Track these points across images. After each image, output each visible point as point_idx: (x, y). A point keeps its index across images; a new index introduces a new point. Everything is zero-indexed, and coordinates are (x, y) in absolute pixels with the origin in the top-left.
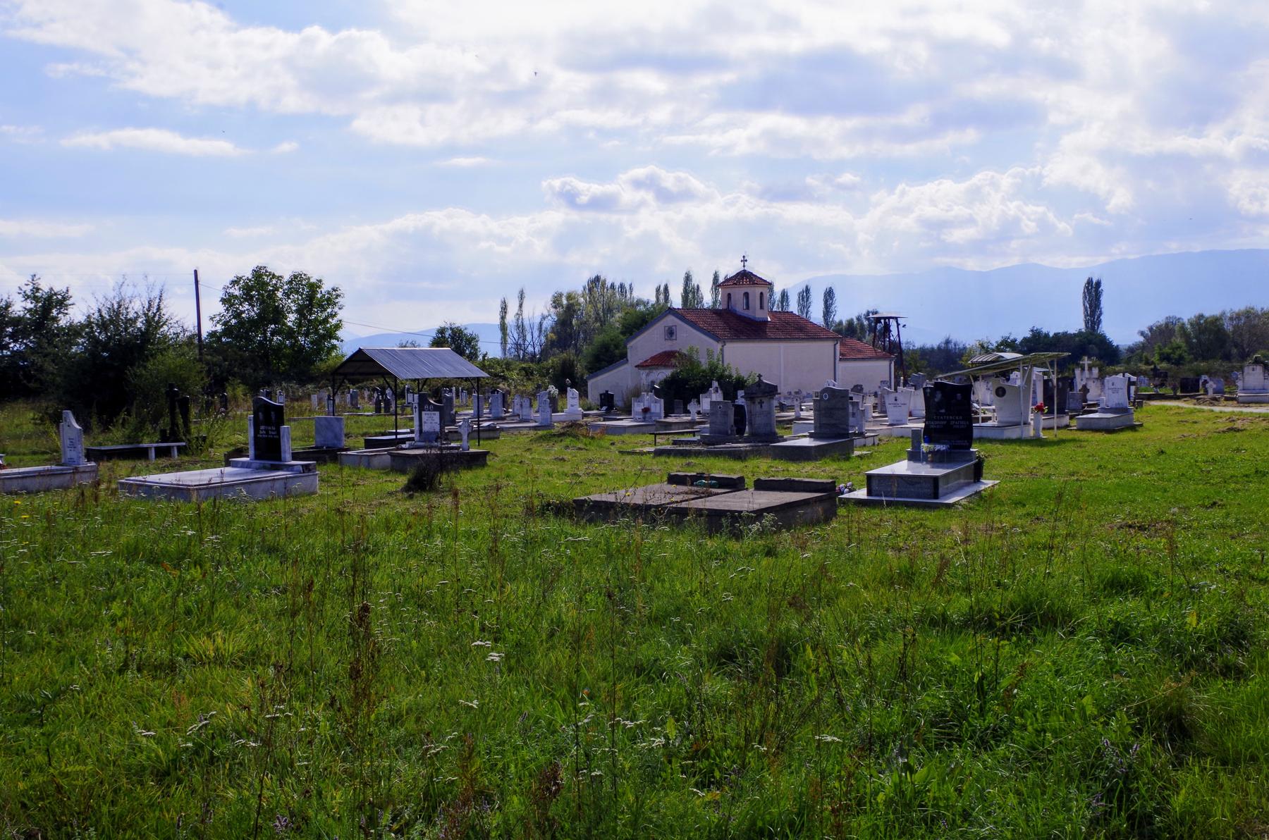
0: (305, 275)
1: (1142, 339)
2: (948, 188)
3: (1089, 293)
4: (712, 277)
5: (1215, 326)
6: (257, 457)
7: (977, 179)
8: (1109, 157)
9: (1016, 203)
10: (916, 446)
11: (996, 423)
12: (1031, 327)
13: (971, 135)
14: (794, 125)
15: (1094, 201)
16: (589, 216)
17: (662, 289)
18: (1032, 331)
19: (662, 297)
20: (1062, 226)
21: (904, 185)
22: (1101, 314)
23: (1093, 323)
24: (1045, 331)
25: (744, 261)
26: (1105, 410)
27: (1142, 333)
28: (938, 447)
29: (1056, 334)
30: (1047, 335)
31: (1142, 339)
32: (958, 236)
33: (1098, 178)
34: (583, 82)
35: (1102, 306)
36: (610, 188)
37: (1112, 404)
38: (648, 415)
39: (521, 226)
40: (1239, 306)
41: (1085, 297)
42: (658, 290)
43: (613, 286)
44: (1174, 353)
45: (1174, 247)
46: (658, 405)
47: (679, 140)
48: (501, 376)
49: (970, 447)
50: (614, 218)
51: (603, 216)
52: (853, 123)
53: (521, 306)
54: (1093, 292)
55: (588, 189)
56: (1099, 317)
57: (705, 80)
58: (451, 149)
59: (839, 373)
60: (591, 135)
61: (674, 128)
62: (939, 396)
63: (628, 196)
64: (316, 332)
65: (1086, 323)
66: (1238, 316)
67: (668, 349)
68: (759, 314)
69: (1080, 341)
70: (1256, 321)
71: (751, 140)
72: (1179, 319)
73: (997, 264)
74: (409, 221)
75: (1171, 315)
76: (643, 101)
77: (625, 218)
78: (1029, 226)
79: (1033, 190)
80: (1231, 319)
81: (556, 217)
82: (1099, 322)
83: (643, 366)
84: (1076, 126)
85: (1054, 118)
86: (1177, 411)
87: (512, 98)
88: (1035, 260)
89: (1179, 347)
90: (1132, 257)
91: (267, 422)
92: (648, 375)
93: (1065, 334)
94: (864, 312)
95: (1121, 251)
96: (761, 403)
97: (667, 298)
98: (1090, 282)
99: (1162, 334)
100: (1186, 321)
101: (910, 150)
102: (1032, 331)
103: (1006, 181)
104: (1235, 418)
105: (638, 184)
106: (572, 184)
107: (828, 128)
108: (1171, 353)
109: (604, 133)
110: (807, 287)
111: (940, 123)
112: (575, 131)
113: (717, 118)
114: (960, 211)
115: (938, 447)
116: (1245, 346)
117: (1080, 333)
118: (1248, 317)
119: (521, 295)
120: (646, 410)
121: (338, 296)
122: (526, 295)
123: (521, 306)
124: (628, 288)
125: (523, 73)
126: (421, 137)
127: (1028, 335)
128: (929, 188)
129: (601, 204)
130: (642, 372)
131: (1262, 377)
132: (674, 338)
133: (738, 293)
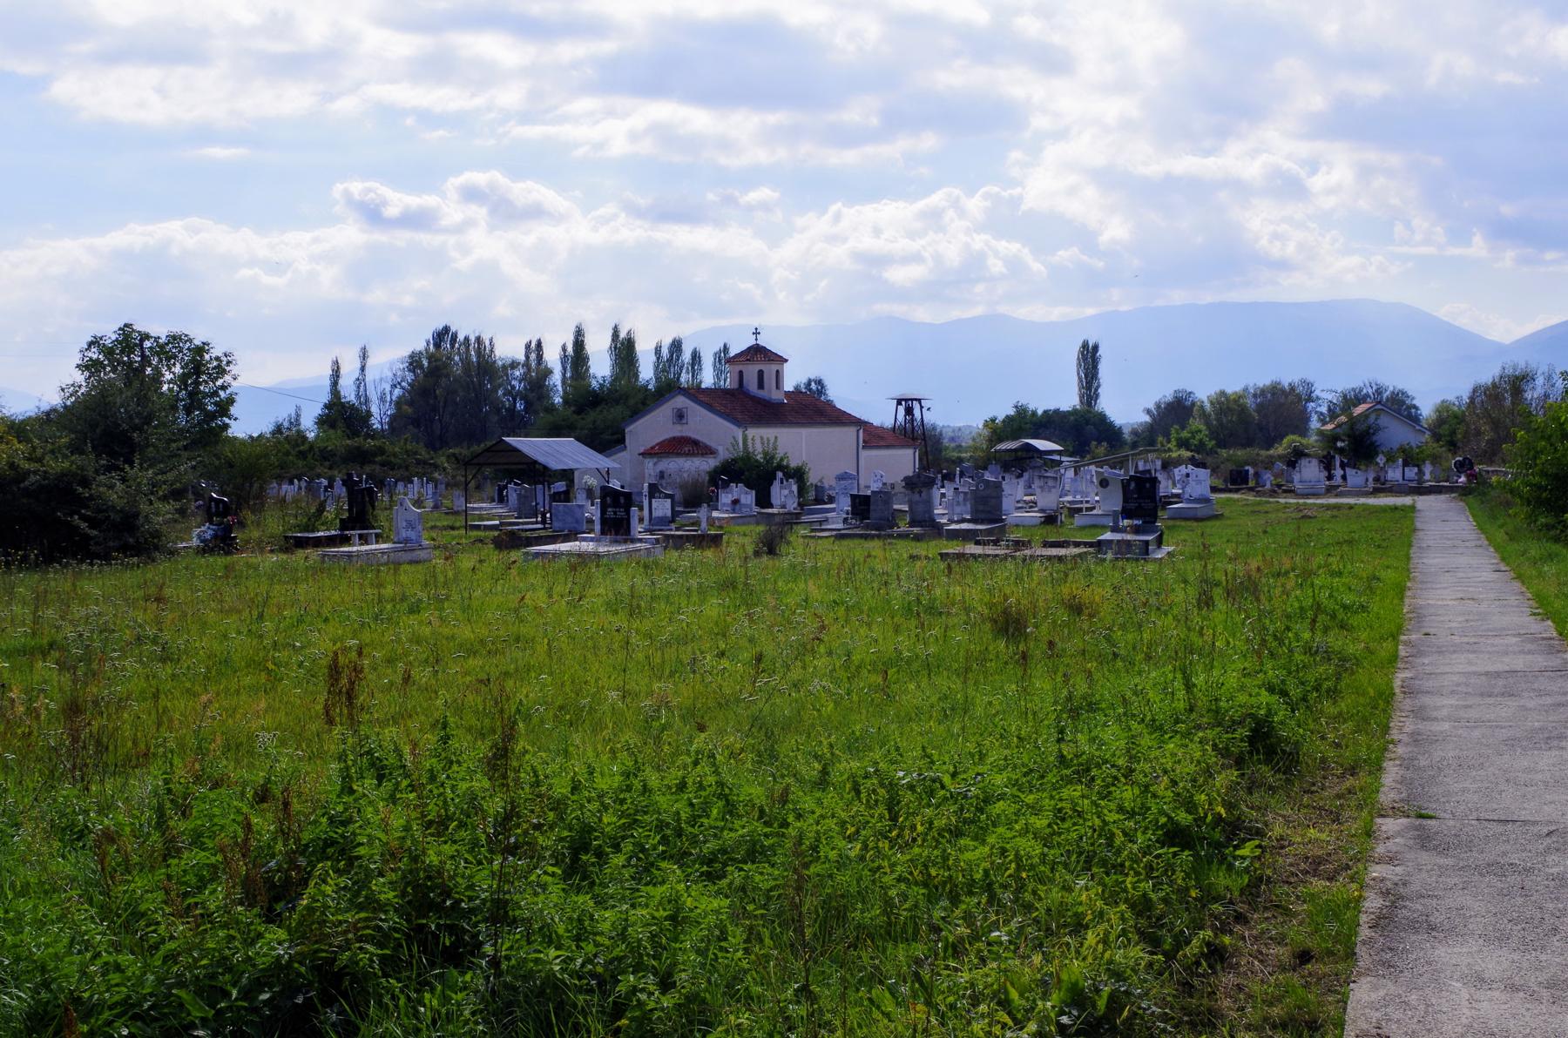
0: (186, 336)
1: (1147, 419)
2: (892, 212)
3: (1085, 359)
4: (610, 332)
5: (1239, 406)
6: (603, 532)
7: (937, 199)
8: (1109, 179)
9: (984, 237)
10: (1116, 522)
11: (1100, 512)
12: (1015, 402)
13: (929, 141)
14: (699, 120)
15: (1084, 237)
16: (402, 237)
17: (533, 345)
18: (1016, 407)
19: (533, 356)
20: (1036, 266)
21: (839, 204)
22: (1098, 386)
23: (1090, 397)
24: (1031, 407)
25: (756, 333)
26: (1189, 501)
27: (1148, 412)
28: (1136, 522)
29: (1045, 412)
30: (1034, 413)
31: (1147, 419)
32: (899, 275)
33: (1086, 205)
34: (404, 46)
35: (1100, 375)
36: (430, 200)
37: (1195, 495)
38: (737, 507)
39: (298, 245)
40: (1263, 380)
41: (1079, 365)
42: (528, 346)
43: (467, 339)
44: (1194, 438)
45: (1178, 297)
46: (749, 497)
47: (534, 131)
48: (431, 464)
49: (1155, 522)
50: (438, 239)
51: (424, 238)
52: (773, 118)
53: (363, 369)
54: (1089, 357)
55: (398, 201)
56: (1096, 390)
57: (568, 51)
58: (204, 134)
59: (862, 463)
60: (410, 121)
61: (526, 118)
62: (1133, 485)
63: (453, 213)
64: (202, 407)
65: (1081, 397)
66: (1263, 392)
67: (678, 434)
68: (776, 396)
69: (1076, 420)
70: (1282, 400)
71: (634, 136)
72: (1190, 393)
73: (956, 314)
74: (133, 236)
75: (1181, 388)
76: (485, 75)
77: (452, 240)
78: (996, 266)
79: (1006, 220)
80: (1255, 396)
81: (350, 235)
82: (1097, 396)
83: (650, 454)
84: (1061, 135)
85: (1040, 122)
86: (1244, 503)
87: (294, 65)
88: (1003, 309)
89: (1200, 431)
90: (1124, 308)
91: (616, 504)
92: (655, 464)
93: (1057, 412)
94: (805, 380)
95: (1120, 300)
96: (920, 492)
97: (540, 357)
98: (1085, 345)
99: (1177, 411)
100: (1205, 399)
101: (850, 157)
102: (1016, 407)
103: (975, 205)
104: (1302, 508)
105: (471, 195)
106: (379, 192)
107: (743, 124)
108: (1190, 438)
109: (427, 118)
110: (725, 346)
111: (894, 123)
112: (388, 114)
113: (586, 104)
114: (904, 245)
115: (1136, 522)
116: (1271, 429)
117: (1075, 412)
118: (1273, 394)
119: (364, 355)
120: (736, 502)
121: (229, 363)
122: (370, 353)
123: (363, 369)
124: (487, 343)
125: (315, 31)
126: (157, 113)
127: (1012, 412)
128: (870, 213)
129: (417, 220)
130: (647, 461)
131: (1317, 469)
132: (684, 421)
133: (751, 371)
